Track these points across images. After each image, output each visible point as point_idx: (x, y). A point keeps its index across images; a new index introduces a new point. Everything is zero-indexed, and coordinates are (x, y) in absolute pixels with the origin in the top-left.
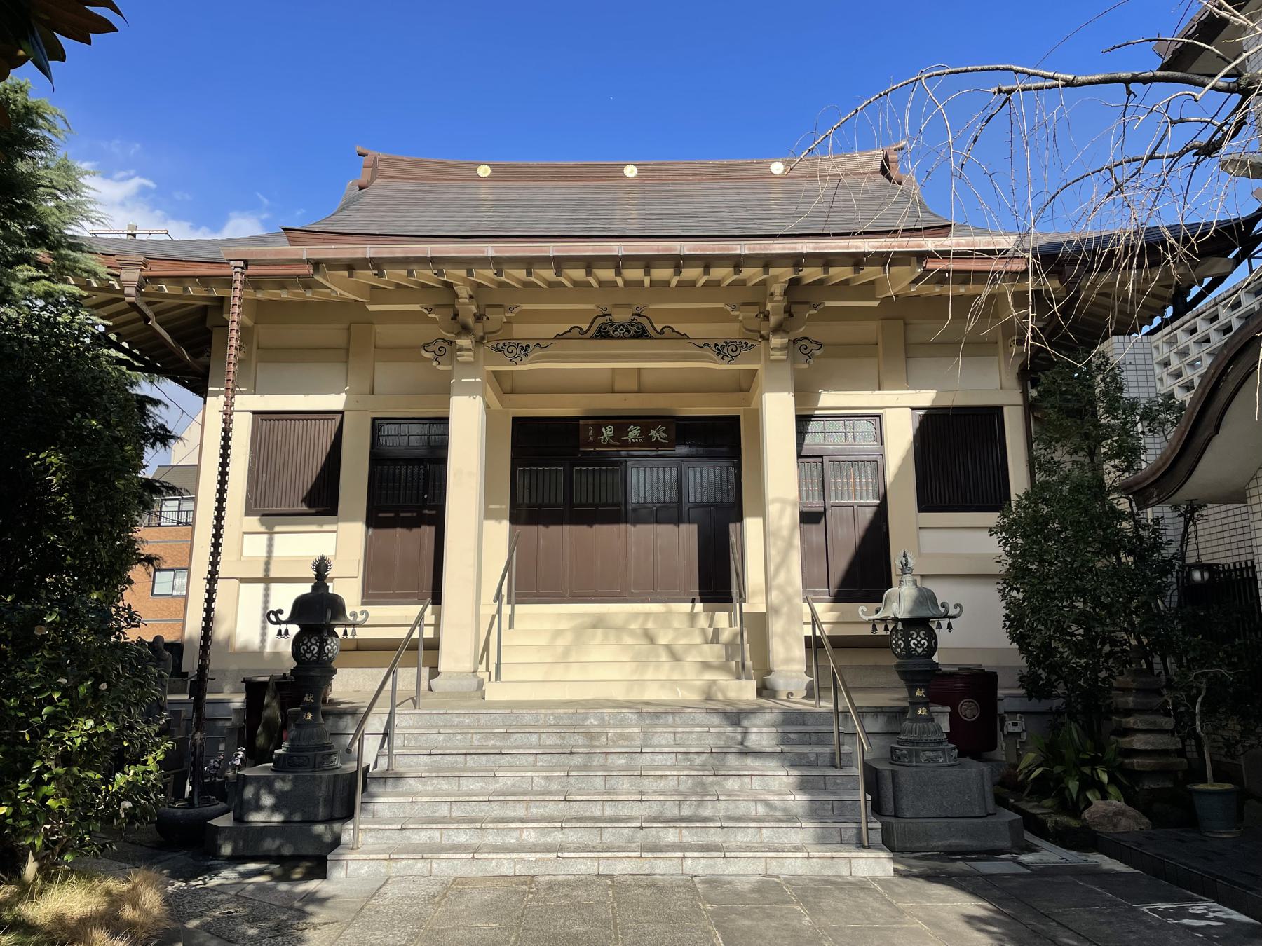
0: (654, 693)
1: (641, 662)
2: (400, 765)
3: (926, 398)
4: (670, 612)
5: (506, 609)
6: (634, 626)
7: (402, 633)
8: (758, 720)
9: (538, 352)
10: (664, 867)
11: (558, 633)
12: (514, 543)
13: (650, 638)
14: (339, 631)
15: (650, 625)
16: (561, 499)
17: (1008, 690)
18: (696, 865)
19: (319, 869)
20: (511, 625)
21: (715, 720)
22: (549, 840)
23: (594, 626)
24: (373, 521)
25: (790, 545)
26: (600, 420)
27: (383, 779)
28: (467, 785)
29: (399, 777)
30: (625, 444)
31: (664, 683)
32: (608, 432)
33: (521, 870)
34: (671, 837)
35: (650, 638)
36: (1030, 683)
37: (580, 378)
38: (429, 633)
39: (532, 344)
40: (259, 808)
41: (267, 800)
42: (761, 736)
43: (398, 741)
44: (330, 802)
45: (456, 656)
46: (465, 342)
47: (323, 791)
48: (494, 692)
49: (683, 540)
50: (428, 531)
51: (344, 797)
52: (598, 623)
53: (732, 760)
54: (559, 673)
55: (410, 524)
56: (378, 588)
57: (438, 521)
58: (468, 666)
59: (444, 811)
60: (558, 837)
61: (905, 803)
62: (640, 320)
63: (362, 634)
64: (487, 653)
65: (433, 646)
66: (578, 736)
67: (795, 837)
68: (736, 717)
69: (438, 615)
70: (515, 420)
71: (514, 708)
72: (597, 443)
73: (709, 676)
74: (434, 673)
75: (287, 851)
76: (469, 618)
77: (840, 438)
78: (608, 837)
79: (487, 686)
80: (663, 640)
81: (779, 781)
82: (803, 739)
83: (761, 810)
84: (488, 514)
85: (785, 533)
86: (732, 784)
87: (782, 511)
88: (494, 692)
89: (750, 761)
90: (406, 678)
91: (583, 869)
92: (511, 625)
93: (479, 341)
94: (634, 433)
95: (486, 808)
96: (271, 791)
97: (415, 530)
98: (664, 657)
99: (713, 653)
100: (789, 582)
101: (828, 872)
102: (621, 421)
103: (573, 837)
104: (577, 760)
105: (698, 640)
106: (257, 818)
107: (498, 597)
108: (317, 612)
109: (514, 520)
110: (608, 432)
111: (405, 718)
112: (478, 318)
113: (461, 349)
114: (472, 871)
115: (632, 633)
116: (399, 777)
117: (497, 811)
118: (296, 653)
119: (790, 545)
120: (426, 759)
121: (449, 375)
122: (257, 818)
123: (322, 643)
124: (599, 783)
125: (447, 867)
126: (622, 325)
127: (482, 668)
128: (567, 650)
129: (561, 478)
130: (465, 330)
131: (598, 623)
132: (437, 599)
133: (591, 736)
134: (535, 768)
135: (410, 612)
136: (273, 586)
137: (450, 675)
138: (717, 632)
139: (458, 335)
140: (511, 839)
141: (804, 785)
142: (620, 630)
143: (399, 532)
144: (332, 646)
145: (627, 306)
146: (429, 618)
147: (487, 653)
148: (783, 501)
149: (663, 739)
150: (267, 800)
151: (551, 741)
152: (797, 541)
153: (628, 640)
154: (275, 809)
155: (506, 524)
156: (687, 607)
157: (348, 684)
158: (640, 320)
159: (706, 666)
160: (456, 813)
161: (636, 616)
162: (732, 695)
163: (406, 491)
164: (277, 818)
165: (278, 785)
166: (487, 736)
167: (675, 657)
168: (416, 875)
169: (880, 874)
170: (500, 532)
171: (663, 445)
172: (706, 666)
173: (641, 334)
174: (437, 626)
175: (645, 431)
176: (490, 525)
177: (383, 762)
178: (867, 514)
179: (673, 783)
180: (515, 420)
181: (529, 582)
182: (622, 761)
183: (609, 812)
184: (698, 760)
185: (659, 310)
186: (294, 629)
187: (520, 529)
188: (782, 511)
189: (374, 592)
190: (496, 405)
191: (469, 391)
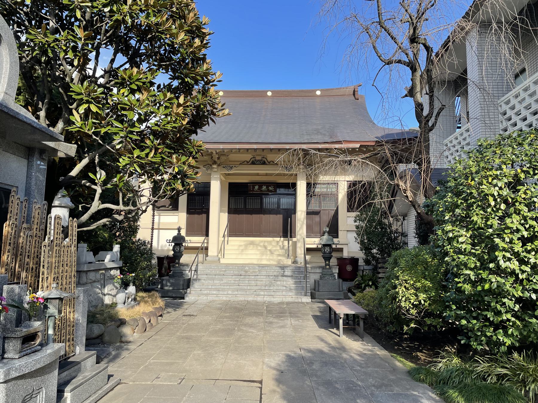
0: (264, 262)
1: (262, 254)
2: (199, 277)
3: (351, 178)
4: (274, 240)
5: (226, 238)
6: (262, 244)
7: (199, 245)
8: (288, 268)
9: (235, 168)
10: (259, 299)
11: (240, 246)
12: (229, 220)
13: (265, 247)
14: (184, 244)
15: (266, 244)
16: (243, 207)
17: (361, 263)
18: (267, 299)
19: (183, 298)
20: (228, 244)
21: (278, 268)
22: (234, 293)
23: (251, 244)
24: (189, 211)
25: (303, 223)
26: (254, 184)
27: (196, 280)
28: (215, 282)
29: (199, 280)
30: (262, 191)
31: (269, 260)
32: (257, 187)
33: (228, 299)
34: (262, 293)
35: (265, 247)
36: (367, 262)
37: (246, 174)
38: (205, 245)
39: (233, 166)
40: (167, 286)
41: (169, 284)
42: (288, 272)
43: (199, 272)
44: (183, 285)
45: (213, 251)
46: (215, 166)
47: (181, 283)
48: (223, 261)
49: (278, 219)
50: (204, 216)
51: (188, 284)
52: (252, 243)
53: (280, 278)
54: (240, 257)
55: (199, 213)
56: (191, 231)
57: (207, 212)
58: (216, 254)
59: (210, 287)
60: (236, 293)
61: (320, 288)
62: (264, 159)
63: (190, 245)
64: (221, 250)
65: (207, 249)
66: (242, 271)
67: (290, 294)
68: (283, 268)
69: (208, 240)
70: (229, 183)
71: (227, 265)
72: (253, 191)
73: (279, 258)
74: (207, 255)
75: (174, 296)
76: (216, 241)
77: (325, 190)
78: (247, 293)
79: (221, 260)
80: (269, 248)
81: (290, 282)
82: (300, 273)
83: (284, 288)
84: (221, 211)
85: (302, 220)
86: (279, 283)
87: (301, 214)
88: (223, 261)
89: (284, 278)
90: (201, 256)
91: (241, 299)
92: (228, 244)
93: (219, 165)
94: (264, 188)
95: (220, 286)
96: (169, 282)
97: (201, 215)
98: (268, 253)
99: (281, 252)
100: (303, 233)
101: (296, 301)
102: (261, 184)
103: (240, 293)
104: (242, 277)
105: (278, 248)
106: (166, 288)
107: (224, 236)
108: (178, 241)
109: (229, 213)
110: (257, 187)
111: (200, 267)
112: (218, 158)
113: (214, 168)
114: (217, 299)
115: (261, 246)
116: (199, 280)
117: (222, 287)
118: (173, 250)
119: (303, 223)
120: (206, 276)
121: (210, 174)
122: (166, 288)
123: (180, 247)
124: (247, 282)
125: (210, 298)
126: (259, 160)
127: (220, 255)
128: (242, 250)
129: (243, 200)
130: (215, 163)
131: (252, 243)
132: (207, 235)
133: (246, 272)
134: (232, 278)
135: (201, 239)
136: (161, 231)
137: (211, 256)
138: (284, 246)
139: (213, 164)
140: (225, 293)
141: (296, 283)
142: (258, 245)
143: (196, 215)
144: (182, 248)
145: (261, 155)
146: (206, 241)
147: (221, 250)
148: (302, 211)
149: (264, 273)
150: (169, 284)
151: (236, 273)
152: (305, 222)
153: (259, 248)
154: (170, 286)
155: (227, 214)
156: (278, 239)
157: (185, 259)
158: (264, 159)
159: (279, 255)
160: (213, 288)
161: (262, 241)
162: (285, 263)
163: (199, 203)
164: (171, 288)
165: (171, 281)
166: (220, 271)
167: (272, 252)
168: (203, 299)
169: (308, 301)
170: (225, 216)
171: (273, 191)
172: (279, 255)
173: (264, 163)
174: (207, 243)
175: (267, 187)
176: (222, 214)
177: (195, 277)
178: (333, 212)
179: (264, 282)
180: (229, 183)
181: (234, 231)
182: (253, 277)
183: (248, 288)
184: (271, 277)
185: (270, 157)
186: (173, 244)
187: (232, 215)
188: (301, 214)
189: (189, 233)
190: (223, 179)
191: (216, 179)
